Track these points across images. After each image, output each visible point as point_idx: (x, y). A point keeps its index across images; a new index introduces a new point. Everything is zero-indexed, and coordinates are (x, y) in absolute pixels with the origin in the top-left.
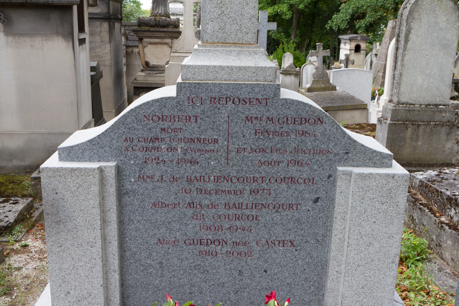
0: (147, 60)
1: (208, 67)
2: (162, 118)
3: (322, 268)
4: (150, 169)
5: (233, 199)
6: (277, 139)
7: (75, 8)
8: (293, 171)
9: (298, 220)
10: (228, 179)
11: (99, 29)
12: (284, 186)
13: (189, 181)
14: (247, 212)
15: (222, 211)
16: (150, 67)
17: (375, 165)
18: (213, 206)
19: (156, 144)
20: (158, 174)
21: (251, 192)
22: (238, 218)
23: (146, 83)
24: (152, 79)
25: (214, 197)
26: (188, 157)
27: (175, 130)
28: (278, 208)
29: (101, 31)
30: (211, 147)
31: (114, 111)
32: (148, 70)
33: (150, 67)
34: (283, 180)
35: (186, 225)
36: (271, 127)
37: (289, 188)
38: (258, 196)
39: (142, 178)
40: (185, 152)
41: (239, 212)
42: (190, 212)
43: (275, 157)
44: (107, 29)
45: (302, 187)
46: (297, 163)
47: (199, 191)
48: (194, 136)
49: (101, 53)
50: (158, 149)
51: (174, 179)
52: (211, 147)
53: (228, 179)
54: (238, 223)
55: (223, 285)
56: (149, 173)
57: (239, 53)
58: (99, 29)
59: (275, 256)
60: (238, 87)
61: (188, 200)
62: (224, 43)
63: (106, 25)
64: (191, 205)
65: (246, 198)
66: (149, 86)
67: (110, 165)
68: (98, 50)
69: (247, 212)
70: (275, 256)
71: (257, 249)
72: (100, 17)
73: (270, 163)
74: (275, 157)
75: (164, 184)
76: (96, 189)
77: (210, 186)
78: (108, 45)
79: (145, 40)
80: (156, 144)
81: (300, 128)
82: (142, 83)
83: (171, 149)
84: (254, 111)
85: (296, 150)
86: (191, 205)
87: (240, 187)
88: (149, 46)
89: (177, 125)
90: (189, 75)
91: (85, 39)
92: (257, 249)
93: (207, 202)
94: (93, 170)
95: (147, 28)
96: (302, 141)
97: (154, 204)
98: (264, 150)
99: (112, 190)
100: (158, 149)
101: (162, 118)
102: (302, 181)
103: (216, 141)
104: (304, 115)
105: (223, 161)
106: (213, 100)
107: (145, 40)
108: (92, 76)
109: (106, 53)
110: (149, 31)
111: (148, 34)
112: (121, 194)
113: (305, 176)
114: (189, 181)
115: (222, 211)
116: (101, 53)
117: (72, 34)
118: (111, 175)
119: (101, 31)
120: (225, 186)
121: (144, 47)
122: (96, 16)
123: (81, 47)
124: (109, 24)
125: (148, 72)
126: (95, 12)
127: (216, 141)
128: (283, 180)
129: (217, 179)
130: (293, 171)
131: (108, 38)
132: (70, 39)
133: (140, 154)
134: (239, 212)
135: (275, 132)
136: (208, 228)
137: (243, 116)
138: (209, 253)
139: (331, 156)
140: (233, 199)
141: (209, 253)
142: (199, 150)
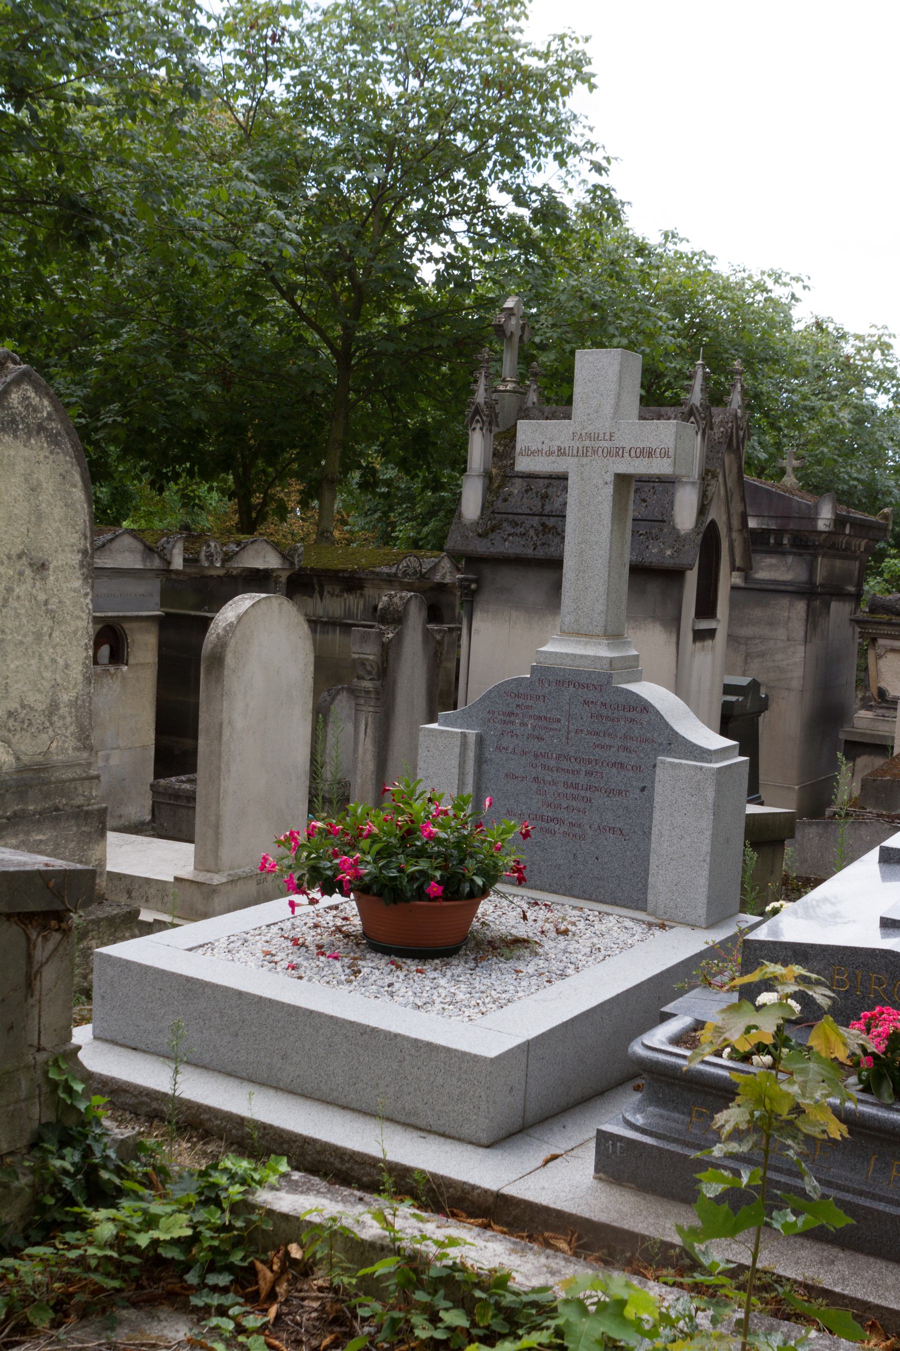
0: (883, 685)
1: (556, 653)
2: (518, 696)
3: (644, 859)
4: (506, 741)
5: (571, 778)
6: (609, 723)
7: (692, 579)
8: (623, 756)
9: (627, 808)
10: (567, 758)
11: (786, 614)
12: (614, 770)
13: (536, 756)
14: (583, 793)
15: (562, 789)
16: (887, 702)
17: (695, 759)
18: (554, 783)
19: (512, 719)
20: (511, 747)
21: (587, 773)
22: (574, 798)
23: (872, 736)
24: (887, 729)
25: (555, 774)
26: (536, 733)
27: (527, 707)
28: (610, 792)
29: (789, 618)
30: (555, 726)
31: (797, 787)
32: (882, 708)
33: (887, 702)
34: (614, 765)
35: (531, 799)
36: (604, 712)
37: (619, 773)
38: (592, 779)
39: (499, 748)
40: (534, 728)
41: (576, 792)
42: (535, 786)
43: (607, 741)
44: (803, 614)
45: (630, 774)
46: (626, 749)
47: (544, 767)
48: (542, 714)
49: (785, 662)
50: (513, 723)
51: (524, 753)
52: (555, 726)
53: (567, 758)
54: (574, 803)
55: (559, 867)
56: (505, 745)
57: (586, 644)
58: (786, 614)
59: (606, 843)
60: (578, 673)
61: (534, 775)
62: (578, 634)
63: (801, 607)
64: (536, 779)
65: (582, 779)
66: (878, 742)
67: (472, 733)
68: (779, 656)
69: (583, 793)
70: (606, 843)
71: (590, 832)
72: (790, 588)
73: (603, 747)
74: (607, 741)
75: (515, 757)
76: (457, 750)
77: (552, 763)
78: (802, 648)
79: (881, 642)
80: (512, 719)
81: (629, 715)
82: (864, 734)
83: (523, 724)
84: (591, 695)
85: (625, 737)
86: (536, 779)
87: (577, 767)
88: (890, 656)
89: (530, 703)
90: (542, 660)
91: (715, 630)
92: (590, 832)
93: (548, 778)
94: (457, 733)
95: (886, 617)
96: (631, 728)
97: (507, 775)
98: (597, 734)
99: (471, 754)
100: (513, 723)
101: (518, 696)
102: (629, 767)
103: (559, 721)
104: (632, 703)
105: (564, 740)
106: (558, 682)
107: (881, 642)
108: (726, 705)
109: (795, 664)
110: (889, 624)
111: (887, 630)
112: (480, 761)
113: (633, 763)
114: (536, 756)
115: (562, 789)
116: (785, 662)
117: (678, 619)
118: (472, 740)
119: (789, 618)
120: (565, 764)
121: (879, 657)
122: (783, 588)
123: (699, 645)
124: (808, 606)
125: (880, 712)
126: (781, 579)
127: (559, 721)
128: (614, 765)
129: (559, 757)
130: (623, 756)
131: (802, 634)
132: (674, 629)
133: (499, 726)
134: (576, 792)
135: (607, 718)
136: (549, 805)
137: (582, 700)
138: (548, 831)
139: (656, 745)
140: (571, 778)
141: (548, 831)
142: (545, 728)
